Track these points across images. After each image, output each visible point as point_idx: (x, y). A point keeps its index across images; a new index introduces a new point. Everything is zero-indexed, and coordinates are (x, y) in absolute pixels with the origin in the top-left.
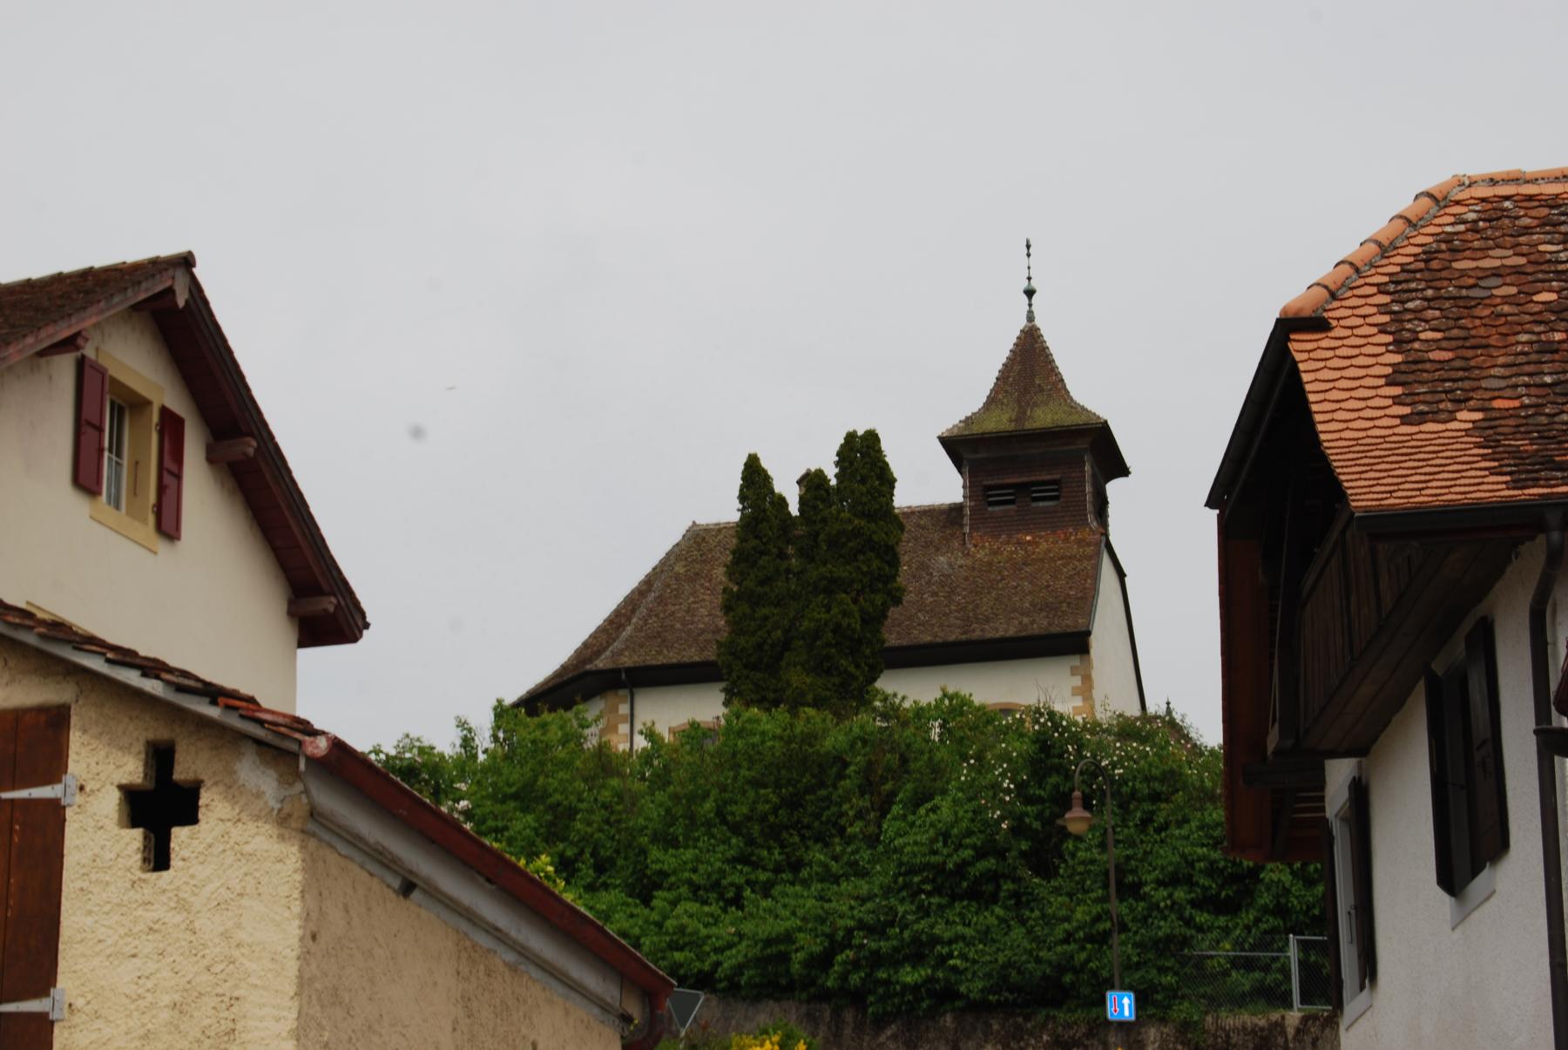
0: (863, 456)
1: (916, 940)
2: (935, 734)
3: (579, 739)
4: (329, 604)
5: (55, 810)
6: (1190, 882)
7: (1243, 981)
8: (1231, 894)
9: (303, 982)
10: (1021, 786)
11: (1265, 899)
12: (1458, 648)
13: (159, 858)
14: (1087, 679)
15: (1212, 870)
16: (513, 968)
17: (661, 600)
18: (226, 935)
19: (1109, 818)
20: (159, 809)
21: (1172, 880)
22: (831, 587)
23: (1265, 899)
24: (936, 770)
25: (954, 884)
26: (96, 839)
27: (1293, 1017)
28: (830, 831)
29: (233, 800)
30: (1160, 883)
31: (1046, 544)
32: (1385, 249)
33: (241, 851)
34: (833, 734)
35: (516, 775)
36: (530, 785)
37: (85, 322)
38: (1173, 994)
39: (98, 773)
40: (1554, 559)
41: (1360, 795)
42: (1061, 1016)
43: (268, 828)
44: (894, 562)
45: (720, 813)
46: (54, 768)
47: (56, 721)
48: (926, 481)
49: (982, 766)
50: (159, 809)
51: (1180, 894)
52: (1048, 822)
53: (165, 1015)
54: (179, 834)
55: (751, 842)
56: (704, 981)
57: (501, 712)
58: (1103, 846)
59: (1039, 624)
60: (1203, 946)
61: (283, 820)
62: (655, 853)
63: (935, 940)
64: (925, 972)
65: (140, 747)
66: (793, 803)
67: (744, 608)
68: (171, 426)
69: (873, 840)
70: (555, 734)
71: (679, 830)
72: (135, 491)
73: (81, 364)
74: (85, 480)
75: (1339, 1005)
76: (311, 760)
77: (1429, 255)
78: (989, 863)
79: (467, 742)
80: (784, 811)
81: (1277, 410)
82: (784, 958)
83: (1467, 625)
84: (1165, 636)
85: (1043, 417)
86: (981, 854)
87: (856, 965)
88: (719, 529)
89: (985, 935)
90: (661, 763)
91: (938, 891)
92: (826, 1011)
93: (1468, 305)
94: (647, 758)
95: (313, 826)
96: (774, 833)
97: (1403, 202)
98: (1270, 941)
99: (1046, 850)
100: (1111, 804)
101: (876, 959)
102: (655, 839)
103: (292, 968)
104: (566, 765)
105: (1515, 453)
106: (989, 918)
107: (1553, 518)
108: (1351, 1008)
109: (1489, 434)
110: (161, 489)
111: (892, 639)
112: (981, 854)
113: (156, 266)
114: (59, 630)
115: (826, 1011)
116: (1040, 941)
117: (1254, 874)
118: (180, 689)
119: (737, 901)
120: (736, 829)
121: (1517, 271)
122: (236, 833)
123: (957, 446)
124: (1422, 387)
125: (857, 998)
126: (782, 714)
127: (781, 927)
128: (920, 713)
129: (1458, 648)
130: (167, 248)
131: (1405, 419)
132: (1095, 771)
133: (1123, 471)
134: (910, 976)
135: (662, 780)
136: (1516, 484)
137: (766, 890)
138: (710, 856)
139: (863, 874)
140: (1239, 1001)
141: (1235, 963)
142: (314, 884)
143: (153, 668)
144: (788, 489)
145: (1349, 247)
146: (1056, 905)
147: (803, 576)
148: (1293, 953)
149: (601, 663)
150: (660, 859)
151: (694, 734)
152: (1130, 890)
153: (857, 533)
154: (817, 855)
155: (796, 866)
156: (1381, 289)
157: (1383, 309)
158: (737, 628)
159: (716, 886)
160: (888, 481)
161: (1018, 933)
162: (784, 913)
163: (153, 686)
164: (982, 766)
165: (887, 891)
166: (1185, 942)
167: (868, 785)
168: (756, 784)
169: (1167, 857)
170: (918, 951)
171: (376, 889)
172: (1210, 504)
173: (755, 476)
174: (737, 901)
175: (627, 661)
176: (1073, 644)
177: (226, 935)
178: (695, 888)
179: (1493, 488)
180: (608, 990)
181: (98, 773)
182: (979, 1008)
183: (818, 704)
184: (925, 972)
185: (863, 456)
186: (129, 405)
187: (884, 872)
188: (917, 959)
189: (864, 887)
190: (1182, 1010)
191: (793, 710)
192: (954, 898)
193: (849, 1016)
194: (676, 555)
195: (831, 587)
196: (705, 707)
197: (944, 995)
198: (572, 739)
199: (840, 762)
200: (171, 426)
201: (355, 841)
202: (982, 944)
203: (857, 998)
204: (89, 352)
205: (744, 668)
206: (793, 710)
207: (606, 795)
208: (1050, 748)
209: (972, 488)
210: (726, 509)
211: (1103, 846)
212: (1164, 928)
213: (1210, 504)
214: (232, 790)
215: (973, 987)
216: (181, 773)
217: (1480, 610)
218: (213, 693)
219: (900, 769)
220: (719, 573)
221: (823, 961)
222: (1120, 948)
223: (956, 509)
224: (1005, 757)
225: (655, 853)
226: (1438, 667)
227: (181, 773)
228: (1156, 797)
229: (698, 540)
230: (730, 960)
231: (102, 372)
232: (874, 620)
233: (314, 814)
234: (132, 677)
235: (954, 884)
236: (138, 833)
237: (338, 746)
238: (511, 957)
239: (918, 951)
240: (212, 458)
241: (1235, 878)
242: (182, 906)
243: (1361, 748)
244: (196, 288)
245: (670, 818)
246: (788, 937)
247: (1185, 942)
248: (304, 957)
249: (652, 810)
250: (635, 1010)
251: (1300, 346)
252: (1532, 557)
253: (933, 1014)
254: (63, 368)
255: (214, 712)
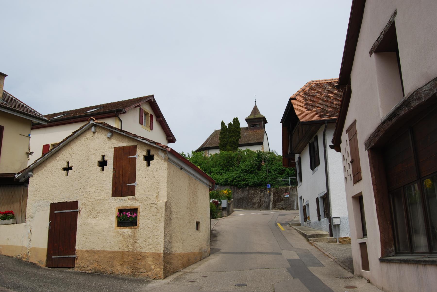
0: (236, 121)
1: (243, 179)
2: (245, 154)
3: (202, 155)
4: (171, 138)
5: (135, 159)
6: (277, 171)
7: (283, 183)
8: (282, 172)
9: (168, 181)
10: (256, 160)
11: (286, 173)
12: (313, 139)
13: (149, 165)
14: (263, 148)
15: (279, 169)
16: (195, 179)
17: (211, 139)
18: (158, 175)
19: (267, 163)
20: (149, 158)
21: (275, 171)
22: (232, 136)
23: (286, 173)
24: (246, 158)
25: (248, 172)
26: (140, 162)
27: (290, 187)
28: (233, 166)
29: (158, 157)
30: (273, 171)
31: (258, 131)
32: (303, 90)
33: (159, 163)
34: (233, 154)
35: (195, 160)
36: (196, 161)
37: (141, 103)
38: (275, 184)
39: (140, 153)
40: (326, 127)
41: (300, 158)
42: (261, 187)
43: (163, 161)
44: (240, 133)
45: (219, 164)
46: (135, 153)
47: (135, 147)
48: (243, 124)
49: (251, 158)
50: (149, 158)
51: (276, 172)
52: (260, 164)
53: (150, 185)
54: (151, 162)
55: (223, 167)
56: (218, 184)
57: (193, 152)
58: (266, 167)
59: (257, 141)
60: (278, 179)
61: (165, 159)
62: (212, 169)
63: (246, 179)
64: (245, 182)
65: (146, 150)
66: (228, 162)
67: (222, 139)
68: (151, 116)
69: (238, 167)
70: (199, 154)
71: (214, 166)
72: (147, 124)
73: (140, 109)
74: (141, 123)
75: (297, 185)
76: (168, 151)
77: (308, 90)
78: (252, 169)
79: (189, 156)
80: (228, 164)
81: (290, 110)
82: (227, 181)
83: (314, 137)
84: (274, 141)
85: (257, 116)
86: (251, 168)
87: (236, 182)
88: (218, 130)
89: (252, 178)
90: (212, 158)
91: (246, 173)
92: (233, 187)
93: (314, 96)
94: (210, 157)
95: (169, 160)
96: (226, 166)
97: (305, 84)
98: (287, 178)
99: (259, 167)
100: (267, 162)
101: (239, 181)
102: (212, 167)
103: (166, 179)
104: (201, 158)
105: (321, 114)
106: (253, 176)
107: (326, 122)
108: (299, 185)
109: (317, 112)
110: (150, 124)
111: (240, 143)
112: (251, 168)
113: (149, 96)
114: (135, 135)
115: (233, 187)
116: (259, 178)
117: (285, 170)
118: (151, 143)
119: (222, 174)
120: (221, 166)
121: (320, 92)
122: (159, 161)
123: (247, 120)
124: (308, 106)
125: (236, 186)
126: (227, 152)
127: (227, 177)
128: (243, 151)
129: (313, 139)
130: (151, 94)
131: (306, 110)
132: (265, 158)
133: (267, 123)
134: (243, 183)
135: (212, 160)
136: (321, 118)
137: (225, 173)
138: (218, 169)
139: (237, 171)
140: (283, 185)
141: (282, 181)
142: (169, 168)
143: (147, 140)
144: (226, 124)
145: (298, 89)
146: (260, 174)
147: (229, 136)
148: (290, 179)
149: (204, 147)
150: (212, 169)
151: (216, 154)
152: (269, 172)
153: (235, 130)
154: (231, 168)
155: (229, 170)
156: (303, 95)
157: (303, 97)
158: (221, 142)
159: (219, 172)
160: (239, 124)
161: (256, 177)
162: (228, 176)
163: (147, 142)
164: (251, 158)
165: (240, 173)
166: (276, 178)
167: (237, 160)
168: (224, 160)
169: (274, 168)
170: (244, 180)
171: (178, 169)
172: (281, 123)
173: (223, 123)
174: (222, 174)
175: (208, 146)
176: (261, 143)
177: (158, 175)
178: (216, 173)
179: (318, 118)
180: (207, 182)
181: (140, 153)
182: (251, 187)
183: (231, 150)
184: (245, 182)
185: (236, 121)
186: (146, 114)
187: (239, 170)
188: (244, 181)
189: (237, 172)
190: (276, 186)
191: (228, 151)
192: (248, 173)
193: (235, 188)
194: (213, 134)
195: (232, 136)
196: (218, 151)
197: (247, 185)
198: (201, 155)
199: (234, 157)
200: (151, 116)
201: (174, 162)
202: (251, 179)
203: (236, 186)
204: (141, 107)
205: (222, 146)
206: (228, 151)
207: (205, 162)
208: (260, 155)
209: (249, 125)
210: (219, 128)
211: (266, 167)
212: (274, 176)
213: (281, 123)
214: (158, 156)
215: (250, 184)
216: (151, 154)
217: (316, 134)
218: (155, 143)
219: (241, 158)
220: (219, 136)
221: (232, 181)
222: (268, 179)
223: (247, 128)
224: (254, 156)
225: (212, 169)
226: (310, 142)
227: (151, 154)
228: (272, 161)
229: (216, 132)
230: (221, 181)
231: (143, 110)
232: (237, 140)
233: (169, 159)
234: (144, 141)
235: (248, 172)
236: (146, 162)
237: (172, 149)
238: (195, 178)
239: (244, 180)
240: (156, 120)
241: (282, 170)
242: (152, 171)
243: (300, 153)
244: (154, 99)
245: (213, 164)
246: (228, 178)
247: (276, 178)
248: (168, 177)
249: (211, 163)
250: (211, 185)
251: (293, 102)
252: (323, 127)
253: (246, 187)
254: (138, 109)
255: (155, 145)
